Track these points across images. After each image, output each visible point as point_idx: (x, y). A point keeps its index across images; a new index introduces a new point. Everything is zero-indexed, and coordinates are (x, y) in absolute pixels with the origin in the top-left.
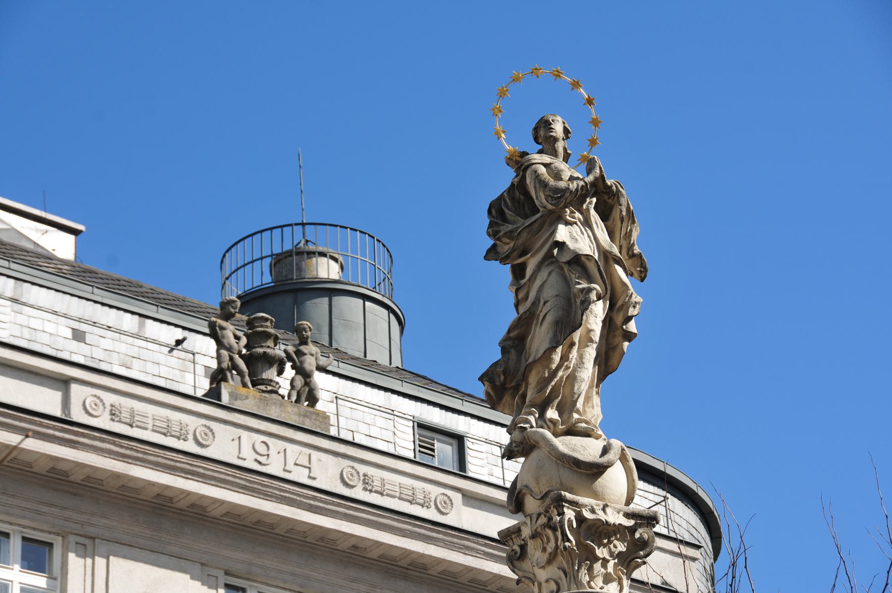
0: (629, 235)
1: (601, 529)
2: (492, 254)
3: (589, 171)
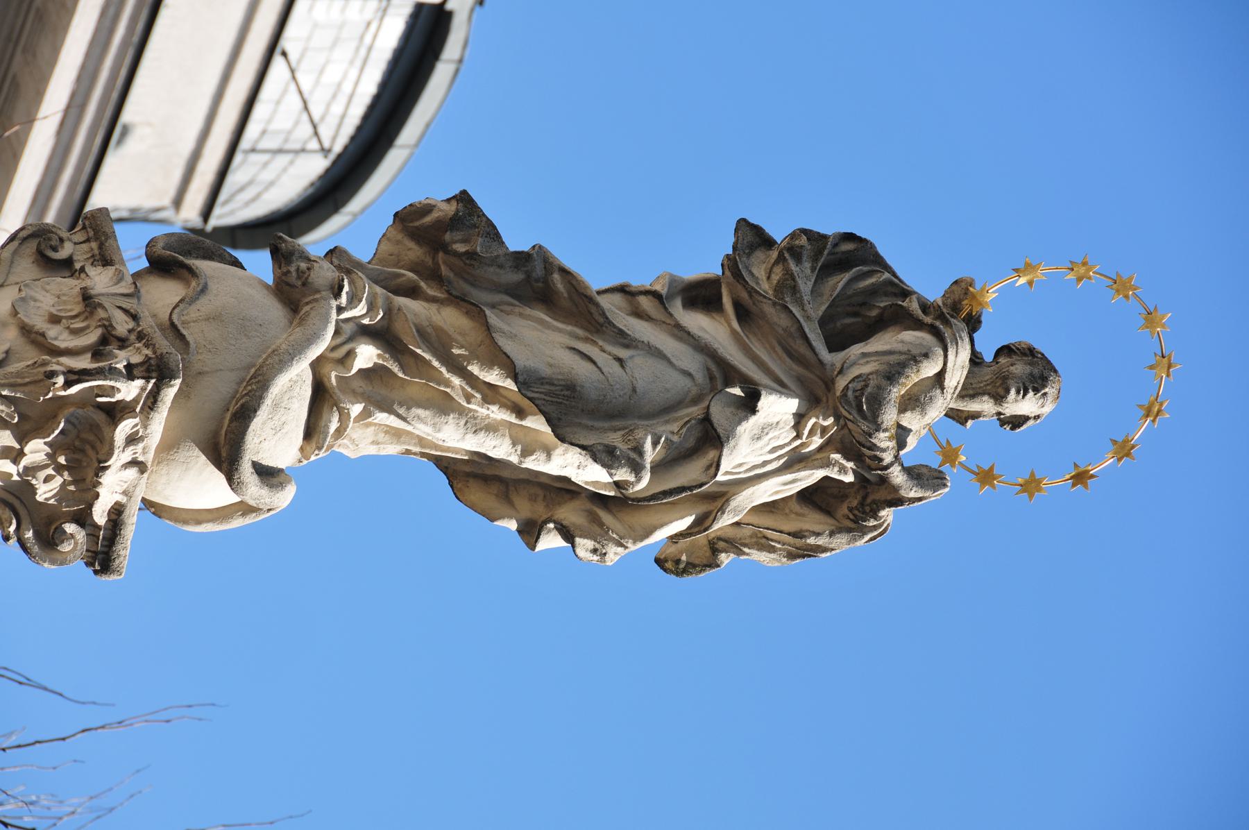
0: (763, 544)
1: (91, 452)
2: (752, 237)
3: (916, 474)
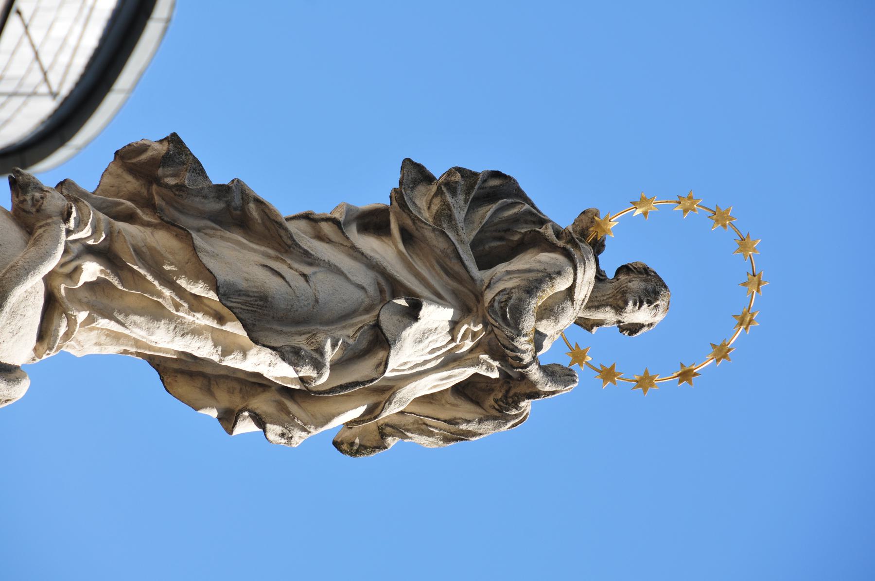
0: (424, 430)
2: (415, 174)
3: (549, 371)
